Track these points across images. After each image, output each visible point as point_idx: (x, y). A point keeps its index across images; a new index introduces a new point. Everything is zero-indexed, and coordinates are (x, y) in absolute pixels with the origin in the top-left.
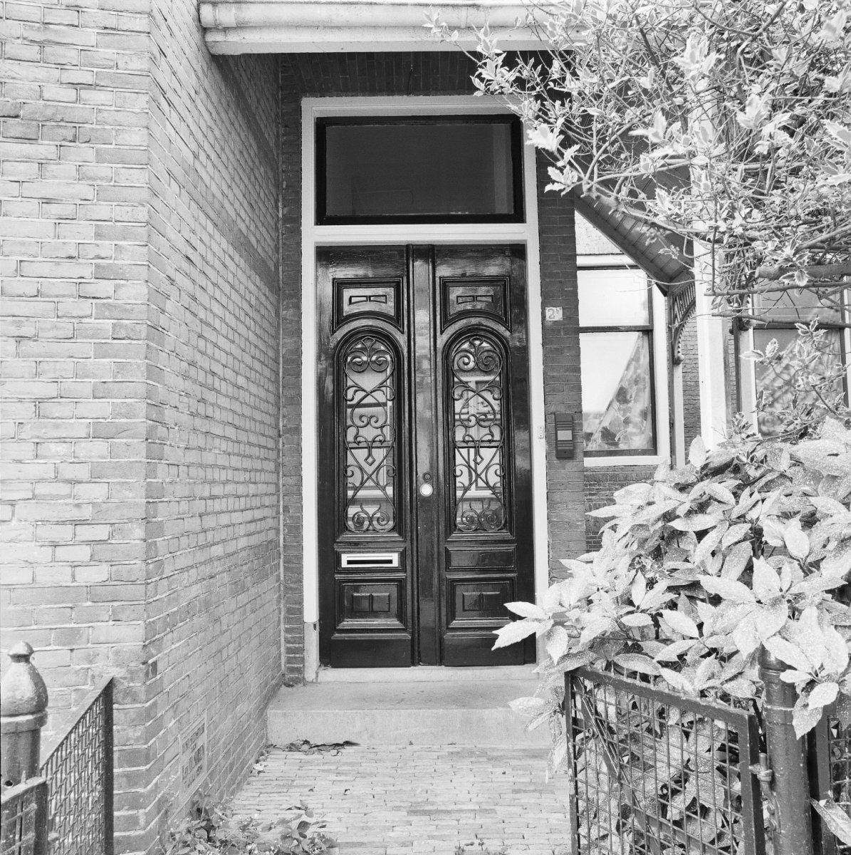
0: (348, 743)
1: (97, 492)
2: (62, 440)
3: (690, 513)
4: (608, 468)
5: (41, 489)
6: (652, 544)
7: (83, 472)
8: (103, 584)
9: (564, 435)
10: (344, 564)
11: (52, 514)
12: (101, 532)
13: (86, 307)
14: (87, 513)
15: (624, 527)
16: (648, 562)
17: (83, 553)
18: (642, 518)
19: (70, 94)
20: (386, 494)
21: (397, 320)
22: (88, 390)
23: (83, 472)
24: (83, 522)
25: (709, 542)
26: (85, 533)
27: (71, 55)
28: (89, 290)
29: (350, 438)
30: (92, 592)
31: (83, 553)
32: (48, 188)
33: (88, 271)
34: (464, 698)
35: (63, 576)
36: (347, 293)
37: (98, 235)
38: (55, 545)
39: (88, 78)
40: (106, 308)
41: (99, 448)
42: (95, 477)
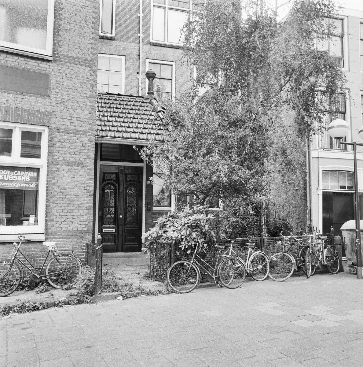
0: (106, 265)
1: (86, 217)
2: (81, 210)
3: (166, 222)
4: (158, 211)
5: (79, 217)
6: (162, 226)
7: (84, 214)
8: (87, 230)
9: (149, 207)
10: (103, 231)
11: (80, 220)
12: (87, 223)
13: (85, 191)
14: (85, 220)
15: (158, 224)
16: (161, 228)
17: (84, 226)
18: (161, 223)
19: (83, 160)
20: (112, 216)
21: (116, 181)
22: (85, 203)
23: (84, 214)
24: (84, 222)
25: (169, 225)
26: (85, 223)
27: (84, 154)
28: (86, 188)
29: (105, 205)
30: (86, 232)
31: (84, 226)
32: (80, 173)
33: (86, 186)
34: (128, 257)
35: (81, 229)
36: (106, 175)
37: (87, 180)
38: (80, 225)
39: (86, 157)
40: (88, 191)
41: (87, 211)
42: (86, 215)
